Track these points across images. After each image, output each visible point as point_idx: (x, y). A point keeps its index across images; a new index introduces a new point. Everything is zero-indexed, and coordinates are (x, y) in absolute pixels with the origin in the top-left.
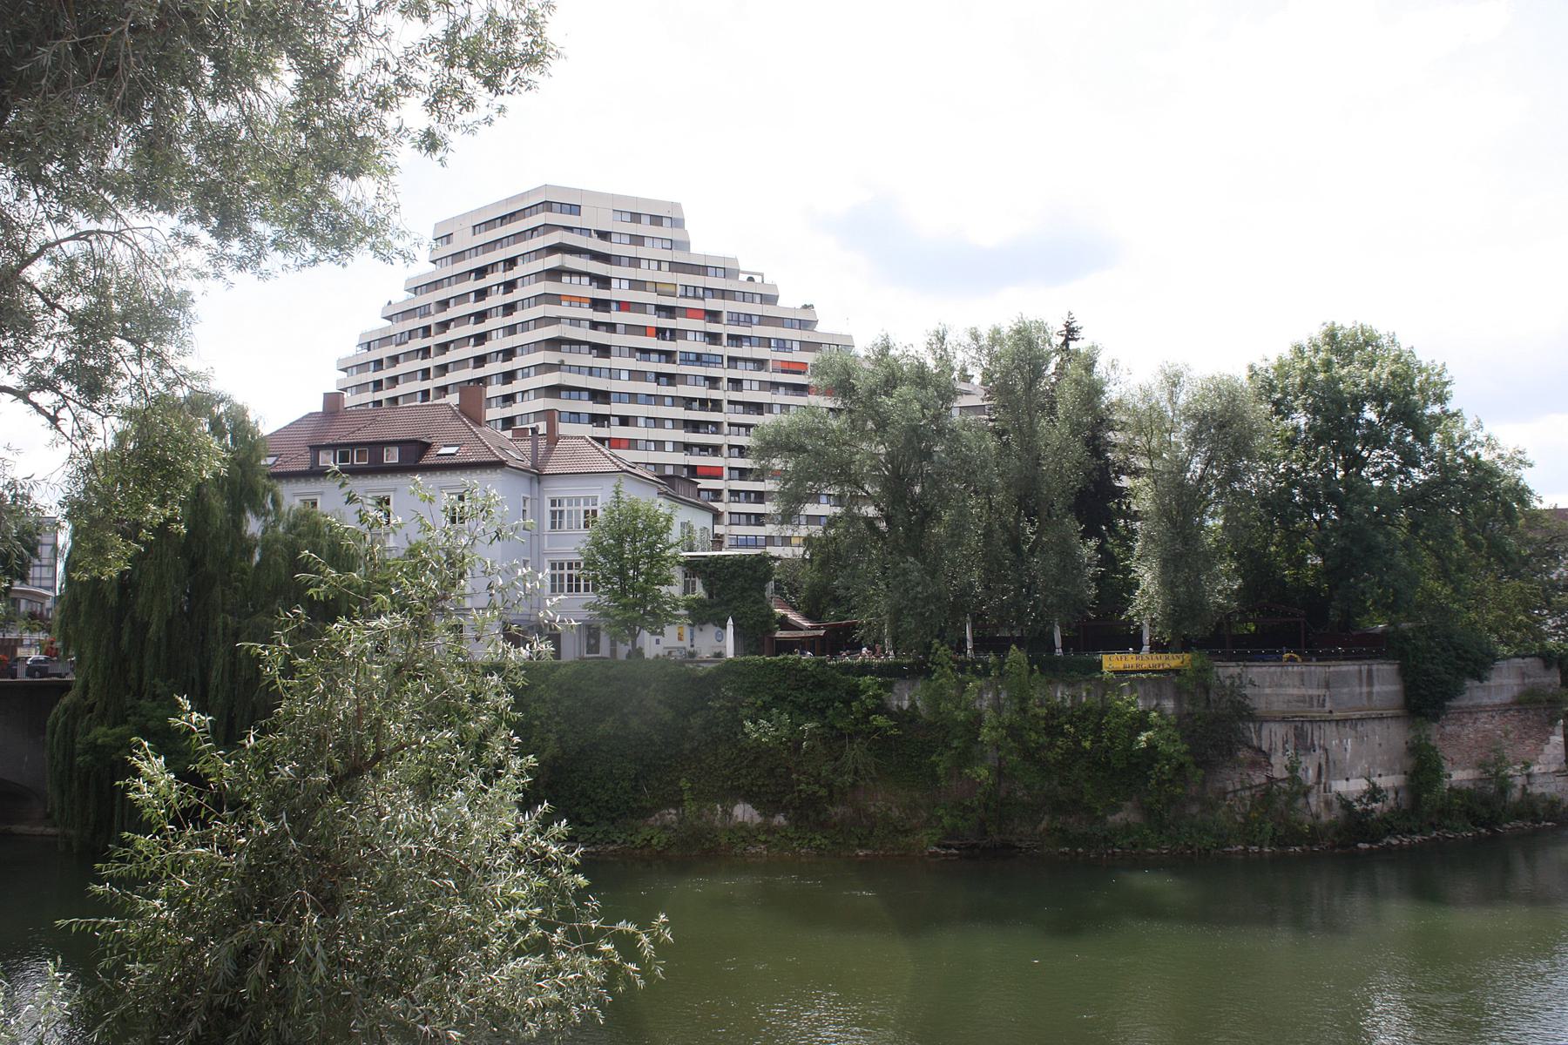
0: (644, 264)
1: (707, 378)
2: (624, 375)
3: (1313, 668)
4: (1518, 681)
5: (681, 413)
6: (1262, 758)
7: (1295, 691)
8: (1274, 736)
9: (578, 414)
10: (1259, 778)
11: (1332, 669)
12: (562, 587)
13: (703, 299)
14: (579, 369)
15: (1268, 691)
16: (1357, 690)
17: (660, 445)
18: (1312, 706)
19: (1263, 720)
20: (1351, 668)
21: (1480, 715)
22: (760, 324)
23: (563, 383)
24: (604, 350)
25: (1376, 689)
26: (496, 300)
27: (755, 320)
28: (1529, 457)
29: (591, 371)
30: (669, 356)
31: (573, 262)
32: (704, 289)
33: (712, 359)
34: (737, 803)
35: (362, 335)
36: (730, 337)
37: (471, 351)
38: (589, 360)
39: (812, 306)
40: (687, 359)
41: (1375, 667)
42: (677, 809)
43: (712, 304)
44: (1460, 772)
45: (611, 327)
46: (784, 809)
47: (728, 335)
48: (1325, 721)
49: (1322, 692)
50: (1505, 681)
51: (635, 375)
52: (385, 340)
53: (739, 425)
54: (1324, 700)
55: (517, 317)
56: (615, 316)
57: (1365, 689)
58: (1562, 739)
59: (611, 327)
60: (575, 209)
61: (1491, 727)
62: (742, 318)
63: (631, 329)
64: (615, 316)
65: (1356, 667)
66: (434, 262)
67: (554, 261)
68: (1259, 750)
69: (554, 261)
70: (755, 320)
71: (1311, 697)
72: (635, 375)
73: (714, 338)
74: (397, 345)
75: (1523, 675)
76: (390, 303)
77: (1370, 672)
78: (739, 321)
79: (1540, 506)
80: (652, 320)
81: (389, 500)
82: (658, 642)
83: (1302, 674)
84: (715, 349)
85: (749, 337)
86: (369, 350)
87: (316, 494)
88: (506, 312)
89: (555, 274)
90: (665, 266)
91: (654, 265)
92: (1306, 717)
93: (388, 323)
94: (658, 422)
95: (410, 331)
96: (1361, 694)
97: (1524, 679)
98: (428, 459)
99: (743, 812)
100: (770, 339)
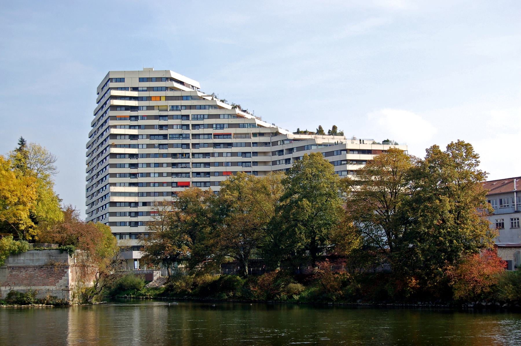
5: (170, 160)
12: (515, 226)
21: (29, 269)
28: (21, 138)
29: (130, 146)
30: (165, 136)
32: (181, 106)
38: (128, 141)
40: (173, 136)
43: (184, 112)
47: (192, 125)
50: (40, 258)
51: (149, 146)
53: (196, 163)
60: (122, 80)
61: (33, 273)
62: (199, 117)
70: (206, 117)
72: (149, 146)
78: (197, 118)
85: (203, 124)
88: (193, 128)
100: (213, 124)
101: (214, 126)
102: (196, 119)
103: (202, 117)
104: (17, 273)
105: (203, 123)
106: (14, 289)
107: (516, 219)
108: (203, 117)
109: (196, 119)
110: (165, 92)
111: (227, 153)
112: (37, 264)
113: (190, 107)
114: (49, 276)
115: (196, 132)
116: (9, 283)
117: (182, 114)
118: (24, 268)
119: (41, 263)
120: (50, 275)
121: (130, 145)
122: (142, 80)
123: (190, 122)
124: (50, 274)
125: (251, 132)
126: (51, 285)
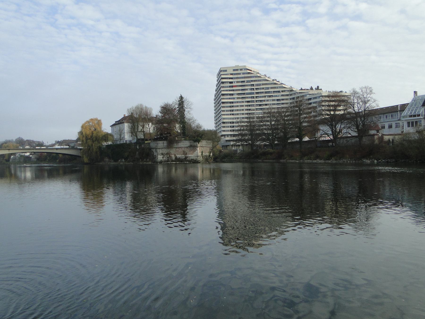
2: (236, 98)
7: (155, 145)
16: (162, 145)
17: (243, 110)
22: (262, 85)
25: (165, 144)
27: (261, 85)
29: (230, 99)
36: (256, 89)
40: (248, 94)
43: (252, 83)
45: (233, 90)
51: (238, 98)
57: (163, 145)
60: (226, 71)
63: (236, 90)
70: (261, 85)
72: (238, 98)
75: (190, 143)
77: (164, 143)
94: (242, 106)
96: (162, 145)
117: (251, 84)
122: (234, 70)
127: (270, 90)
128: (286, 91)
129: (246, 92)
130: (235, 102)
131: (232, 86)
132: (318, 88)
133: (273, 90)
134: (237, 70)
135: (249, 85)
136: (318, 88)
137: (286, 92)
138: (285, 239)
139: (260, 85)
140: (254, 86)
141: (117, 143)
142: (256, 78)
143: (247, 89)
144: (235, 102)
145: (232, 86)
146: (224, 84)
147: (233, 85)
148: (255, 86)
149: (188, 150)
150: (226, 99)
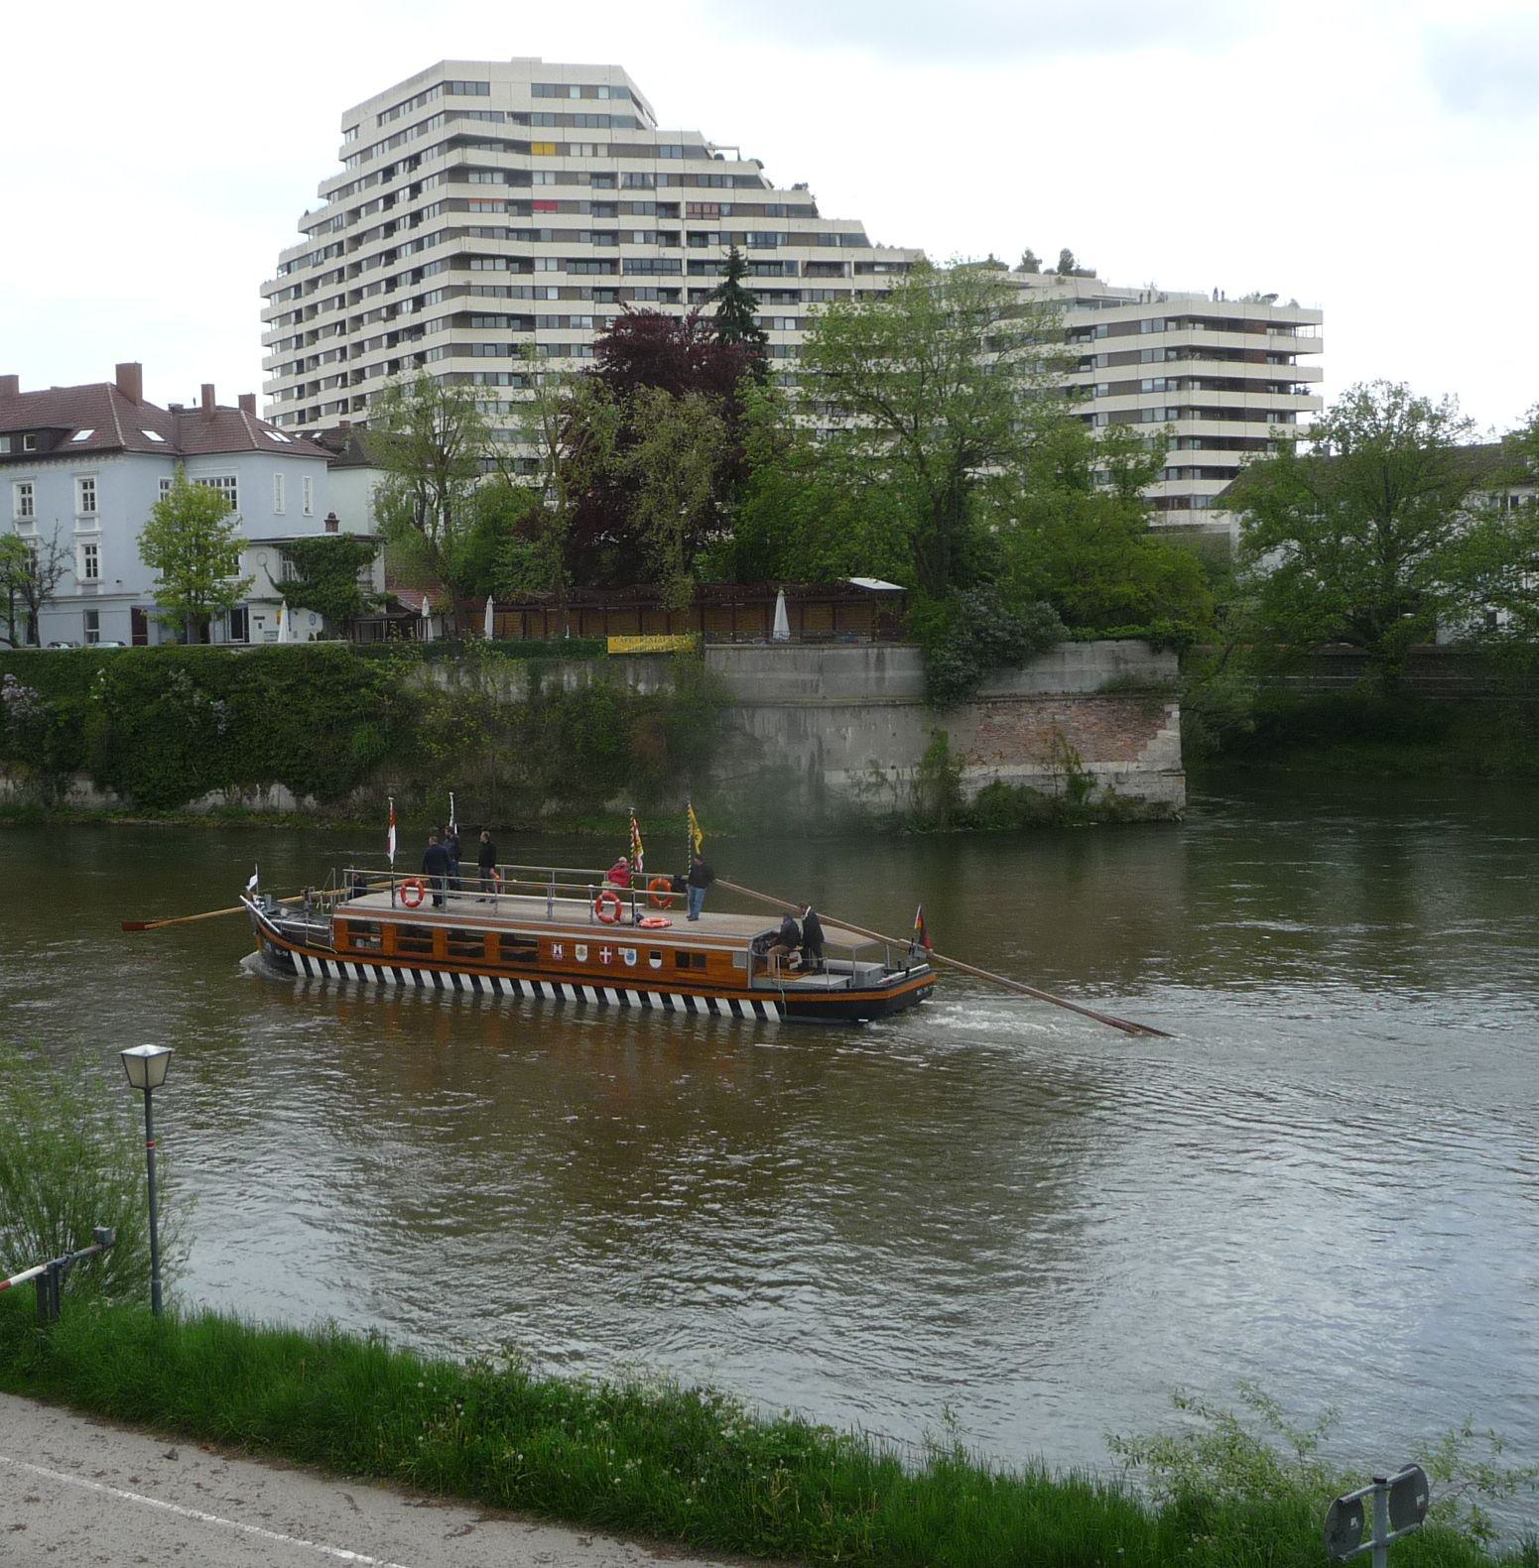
0: (575, 151)
1: (661, 290)
2: (553, 294)
3: (806, 651)
4: (1110, 667)
6: (754, 745)
8: (765, 724)
9: (495, 345)
10: (753, 767)
11: (826, 652)
13: (654, 188)
14: (494, 291)
15: (760, 675)
18: (805, 692)
19: (752, 705)
20: (854, 651)
22: (731, 215)
23: (469, 309)
24: (526, 264)
25: (890, 673)
26: (403, 207)
29: (509, 291)
30: (612, 265)
31: (475, 156)
32: (655, 175)
33: (667, 265)
34: (273, 783)
35: (282, 255)
36: (691, 235)
37: (382, 272)
39: (806, 185)
41: (888, 651)
42: (223, 788)
44: (1012, 767)
45: (534, 235)
46: (312, 789)
48: (817, 708)
49: (814, 677)
50: (1086, 667)
51: (566, 293)
52: (304, 259)
54: (817, 685)
55: (425, 228)
56: (540, 221)
57: (873, 674)
58: (1178, 734)
59: (534, 235)
60: (481, 89)
61: (1063, 718)
62: (706, 209)
63: (559, 235)
64: (540, 221)
65: (861, 651)
66: (344, 160)
67: (454, 158)
68: (752, 737)
69: (454, 158)
71: (804, 683)
72: (566, 293)
73: (672, 238)
74: (314, 266)
75: (1117, 660)
76: (307, 213)
77: (880, 659)
78: (702, 213)
79: (1462, 440)
80: (586, 222)
81: (30, 489)
82: (260, 626)
83: (795, 657)
84: (671, 253)
86: (289, 272)
87: (94, 473)
89: (458, 173)
90: (602, 151)
91: (588, 151)
92: (798, 703)
93: (305, 237)
95: (326, 249)
97: (1117, 664)
98: (64, 448)
99: (280, 796)
100: (745, 234)
101: (750, 239)
102: (699, 216)
103: (715, 210)
104: (1009, 719)
105: (718, 230)
106: (999, 774)
107: (223, 482)
108: (716, 211)
109: (699, 216)
110: (609, 131)
111: (785, 318)
112: (1074, 689)
113: (681, 180)
114: (1114, 729)
115: (698, 254)
116: (982, 753)
117: (659, 200)
118: (1031, 701)
119: (1089, 685)
120: (1119, 726)
121: (509, 288)
122: (540, 90)
123: (680, 225)
124: (1117, 720)
125: (853, 260)
126: (1123, 758)
127: (782, 253)
128: (876, 269)
129: (624, 251)
130: (548, 322)
131: (525, 207)
132: (1066, 265)
133: (801, 254)
134: (561, 91)
135: (643, 209)
136: (1066, 265)
137: (878, 273)
138: (1096, 1308)
139: (720, 214)
140: (677, 217)
141: (33, 637)
142: (689, 163)
143: (627, 236)
144: (548, 322)
145: (525, 207)
146: (467, 181)
147: (535, 198)
148: (683, 214)
149: (1092, 719)
150: (483, 291)
